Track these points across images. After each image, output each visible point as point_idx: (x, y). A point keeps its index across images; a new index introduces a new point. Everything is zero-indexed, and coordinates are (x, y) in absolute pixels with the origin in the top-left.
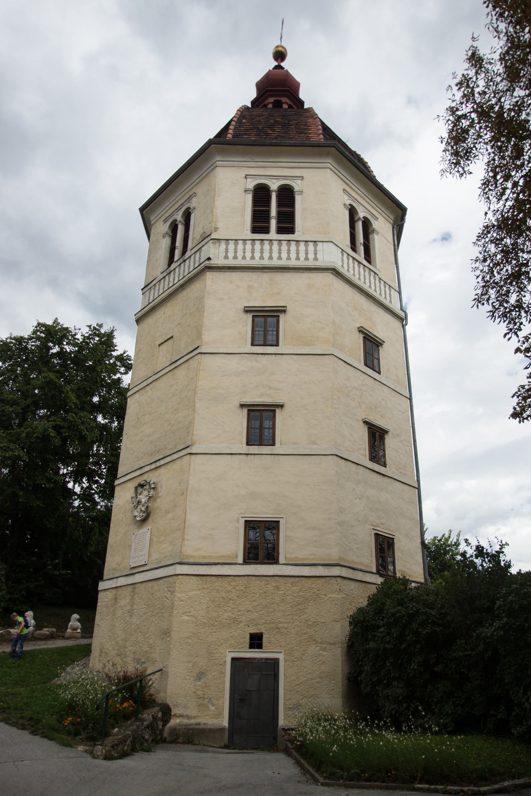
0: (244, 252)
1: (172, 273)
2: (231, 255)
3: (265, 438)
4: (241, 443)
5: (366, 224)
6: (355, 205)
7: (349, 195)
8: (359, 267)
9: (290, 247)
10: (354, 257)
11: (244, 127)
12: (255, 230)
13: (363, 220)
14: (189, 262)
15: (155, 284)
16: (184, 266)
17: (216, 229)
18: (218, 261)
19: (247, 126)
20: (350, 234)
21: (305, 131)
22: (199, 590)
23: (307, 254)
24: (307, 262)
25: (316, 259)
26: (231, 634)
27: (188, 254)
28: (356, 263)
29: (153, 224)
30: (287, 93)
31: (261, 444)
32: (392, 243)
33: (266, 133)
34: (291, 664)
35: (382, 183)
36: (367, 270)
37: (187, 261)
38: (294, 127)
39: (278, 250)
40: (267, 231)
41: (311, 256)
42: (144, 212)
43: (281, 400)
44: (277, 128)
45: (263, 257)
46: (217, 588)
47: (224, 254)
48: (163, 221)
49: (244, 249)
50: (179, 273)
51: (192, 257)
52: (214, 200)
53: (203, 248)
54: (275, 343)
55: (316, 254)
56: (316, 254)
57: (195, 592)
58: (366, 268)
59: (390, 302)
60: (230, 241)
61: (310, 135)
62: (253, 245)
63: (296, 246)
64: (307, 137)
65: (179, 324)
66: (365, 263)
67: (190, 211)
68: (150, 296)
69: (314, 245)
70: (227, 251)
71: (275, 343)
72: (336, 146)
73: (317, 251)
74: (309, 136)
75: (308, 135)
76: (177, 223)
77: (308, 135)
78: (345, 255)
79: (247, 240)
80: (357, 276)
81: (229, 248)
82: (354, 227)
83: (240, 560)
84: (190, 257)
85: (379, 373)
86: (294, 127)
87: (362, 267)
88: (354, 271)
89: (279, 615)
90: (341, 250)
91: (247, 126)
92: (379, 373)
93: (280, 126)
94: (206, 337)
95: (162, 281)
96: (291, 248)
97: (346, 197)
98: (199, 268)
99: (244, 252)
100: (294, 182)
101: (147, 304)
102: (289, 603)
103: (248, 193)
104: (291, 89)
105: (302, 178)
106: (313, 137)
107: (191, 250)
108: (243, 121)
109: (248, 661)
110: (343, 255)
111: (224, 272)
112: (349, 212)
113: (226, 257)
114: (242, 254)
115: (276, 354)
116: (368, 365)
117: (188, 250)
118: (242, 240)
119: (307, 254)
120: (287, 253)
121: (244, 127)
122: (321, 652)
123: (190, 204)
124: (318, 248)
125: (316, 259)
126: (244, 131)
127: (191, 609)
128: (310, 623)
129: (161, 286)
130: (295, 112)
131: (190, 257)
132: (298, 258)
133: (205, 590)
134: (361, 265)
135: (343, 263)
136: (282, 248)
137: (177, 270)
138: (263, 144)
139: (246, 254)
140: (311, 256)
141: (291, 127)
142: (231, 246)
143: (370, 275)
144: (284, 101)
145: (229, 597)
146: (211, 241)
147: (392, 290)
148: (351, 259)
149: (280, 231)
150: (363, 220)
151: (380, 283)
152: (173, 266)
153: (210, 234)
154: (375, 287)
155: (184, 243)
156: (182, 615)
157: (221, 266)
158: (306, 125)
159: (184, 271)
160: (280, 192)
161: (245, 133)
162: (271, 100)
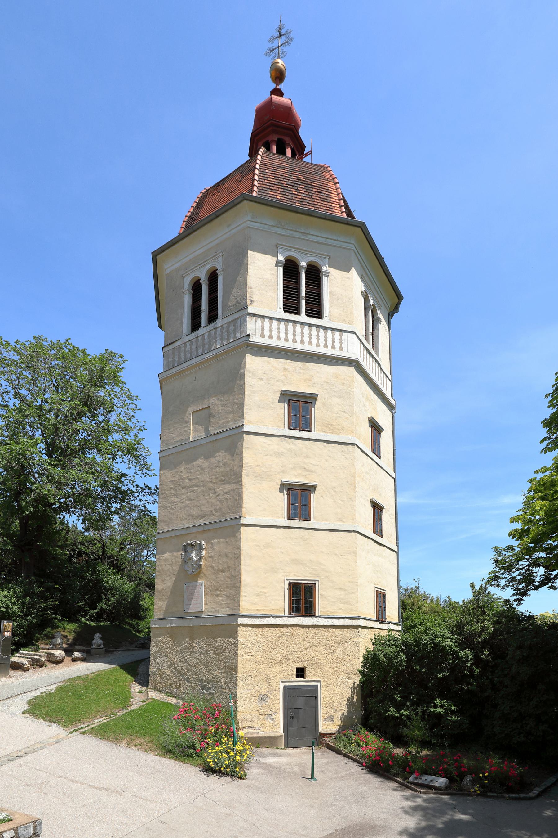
12: (287, 309)
15: (179, 346)
22: (257, 636)
25: (341, 349)
26: (283, 669)
34: (326, 689)
38: (316, 190)
41: (337, 345)
45: (296, 339)
46: (271, 634)
55: (341, 343)
56: (341, 343)
57: (254, 638)
69: (293, 325)
70: (263, 328)
74: (331, 206)
75: (330, 204)
77: (330, 204)
83: (287, 613)
89: (317, 654)
96: (320, 334)
102: (324, 646)
116: (164, 349)
122: (347, 680)
123: (216, 263)
124: (343, 337)
127: (251, 650)
128: (340, 659)
133: (261, 636)
140: (337, 345)
145: (280, 641)
156: (245, 655)
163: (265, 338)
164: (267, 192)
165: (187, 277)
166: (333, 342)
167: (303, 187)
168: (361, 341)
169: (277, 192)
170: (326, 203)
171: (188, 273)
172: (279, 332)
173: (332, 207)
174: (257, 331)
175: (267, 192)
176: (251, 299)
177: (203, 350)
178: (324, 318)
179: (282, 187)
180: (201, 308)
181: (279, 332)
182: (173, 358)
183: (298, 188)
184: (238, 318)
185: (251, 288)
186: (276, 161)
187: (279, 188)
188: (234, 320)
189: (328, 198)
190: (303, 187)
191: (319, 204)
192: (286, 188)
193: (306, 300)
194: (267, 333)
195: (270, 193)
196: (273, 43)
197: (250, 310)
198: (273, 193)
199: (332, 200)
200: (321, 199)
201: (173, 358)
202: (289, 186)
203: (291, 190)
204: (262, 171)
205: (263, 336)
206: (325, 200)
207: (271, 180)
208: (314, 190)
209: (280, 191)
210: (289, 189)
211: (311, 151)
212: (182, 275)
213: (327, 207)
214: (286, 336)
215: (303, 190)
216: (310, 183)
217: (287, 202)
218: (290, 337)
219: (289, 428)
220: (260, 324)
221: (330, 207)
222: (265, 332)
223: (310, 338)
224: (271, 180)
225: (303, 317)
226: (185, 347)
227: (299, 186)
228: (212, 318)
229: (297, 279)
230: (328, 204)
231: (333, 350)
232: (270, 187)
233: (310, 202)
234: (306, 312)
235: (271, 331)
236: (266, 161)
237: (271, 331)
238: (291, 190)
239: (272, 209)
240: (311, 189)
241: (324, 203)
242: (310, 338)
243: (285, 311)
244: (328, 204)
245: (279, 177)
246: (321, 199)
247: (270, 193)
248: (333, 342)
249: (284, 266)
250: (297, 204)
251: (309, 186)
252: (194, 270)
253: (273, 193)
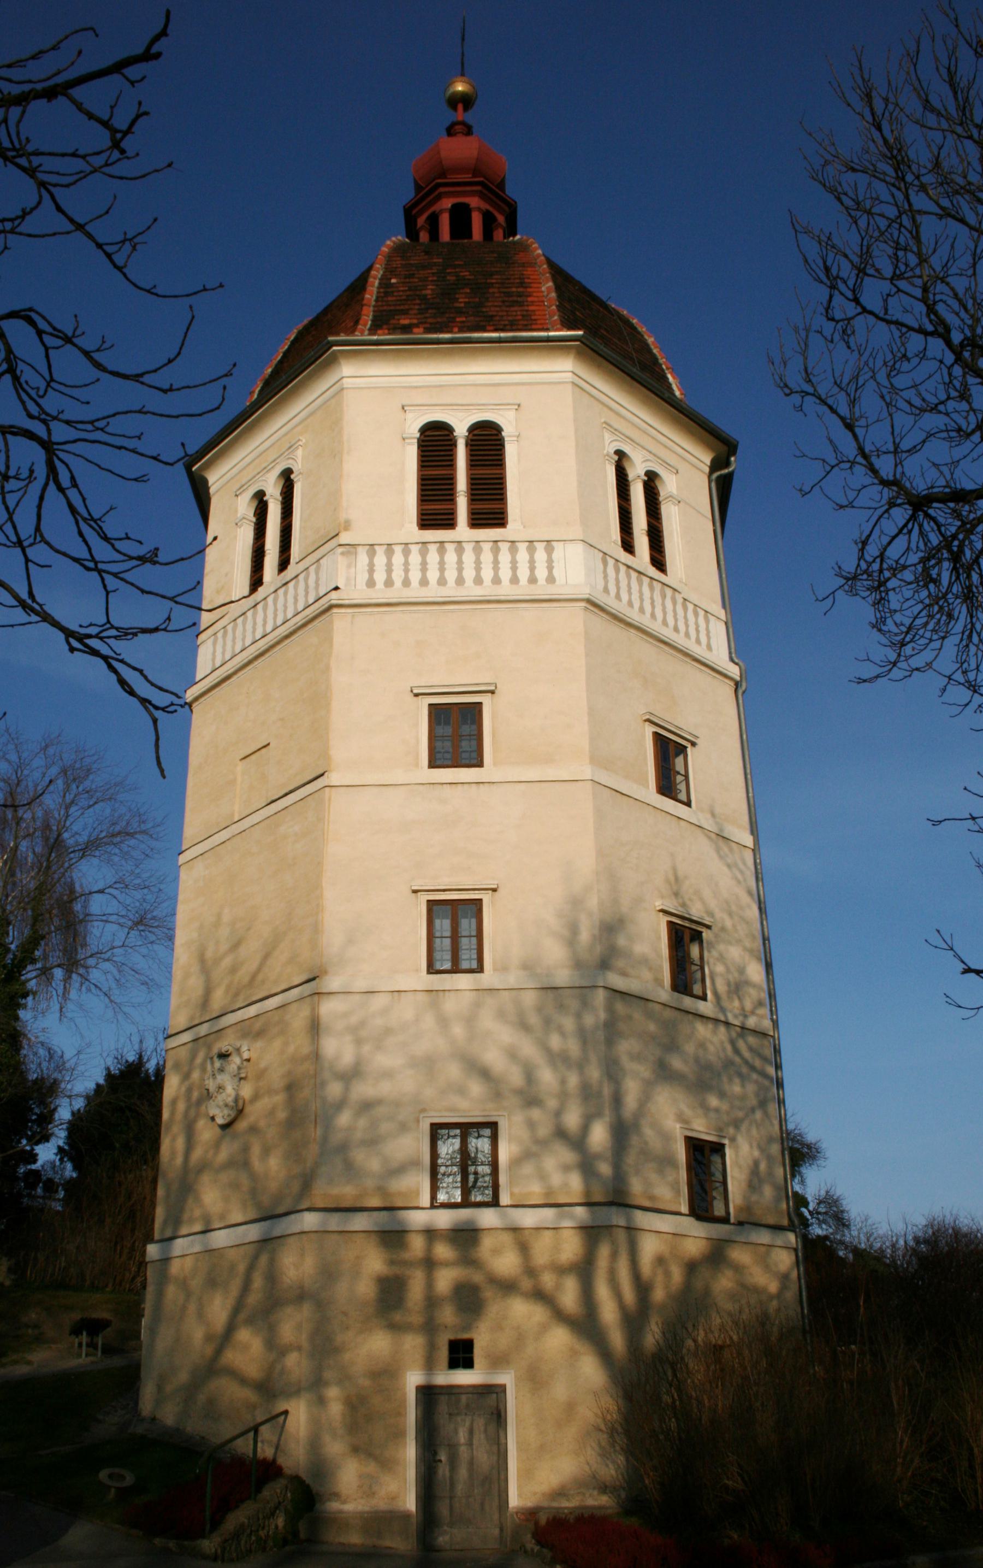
0: (407, 571)
1: (260, 607)
2: (380, 577)
3: (464, 933)
4: (417, 970)
5: (651, 483)
6: (627, 449)
7: (615, 431)
8: (640, 584)
10: (630, 564)
11: (395, 294)
13: (646, 478)
14: (296, 588)
16: (286, 594)
17: (347, 526)
18: (356, 592)
19: (401, 293)
20: (620, 512)
21: (519, 299)
23: (532, 568)
24: (533, 586)
25: (551, 579)
27: (292, 570)
28: (634, 575)
29: (214, 494)
30: (479, 188)
31: (456, 763)
32: (710, 517)
36: (657, 586)
37: (291, 585)
39: (475, 562)
40: (448, 522)
41: (541, 573)
42: (194, 469)
44: (463, 296)
47: (366, 576)
49: (406, 564)
50: (276, 610)
51: (301, 577)
52: (342, 461)
53: (322, 561)
54: (474, 965)
55: (550, 568)
56: (550, 568)
58: (655, 583)
59: (709, 647)
60: (376, 547)
61: (531, 308)
62: (424, 553)
64: (525, 313)
65: (282, 719)
66: (653, 571)
67: (292, 477)
68: (214, 652)
71: (474, 965)
73: (552, 561)
74: (527, 311)
76: (265, 499)
78: (611, 562)
80: (637, 605)
82: (629, 495)
84: (297, 576)
85: (688, 804)
86: (496, 290)
87: (646, 581)
88: (630, 593)
90: (601, 554)
91: (401, 293)
92: (688, 804)
93: (468, 291)
94: (340, 751)
95: (240, 621)
97: (608, 437)
98: (317, 605)
99: (407, 571)
100: (502, 416)
101: (209, 672)
103: (409, 444)
104: (487, 179)
105: (516, 407)
106: (537, 313)
107: (297, 563)
108: (393, 281)
109: (439, 707)
110: (605, 563)
112: (616, 470)
113: (371, 583)
114: (403, 574)
117: (293, 559)
119: (532, 568)
120: (493, 568)
121: (395, 294)
124: (555, 556)
125: (551, 579)
126: (396, 305)
129: (237, 632)
131: (297, 576)
132: (515, 580)
134: (645, 579)
135: (606, 582)
136: (482, 558)
137: (270, 600)
139: (411, 574)
140: (541, 573)
141: (491, 290)
142: (380, 559)
143: (664, 596)
146: (340, 550)
147: (712, 619)
148: (623, 569)
149: (479, 520)
150: (646, 478)
151: (685, 609)
152: (262, 592)
153: (337, 535)
154: (676, 620)
155: (281, 541)
158: (522, 284)
159: (285, 607)
160: (474, 435)
161: (398, 308)
162: (447, 203)
228: (284, 564)
246: (507, 304)
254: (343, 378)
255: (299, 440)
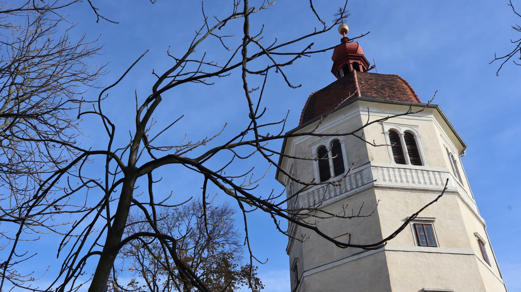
9: (424, 174)
33: (381, 92)
35: (214, 72)
38: (397, 89)
43: (450, 288)
48: (400, 159)
63: (428, 175)
72: (437, 108)
79: (395, 168)
81: (436, 177)
111: (386, 190)
115: (437, 253)
118: (392, 168)
124: (442, 176)
130: (391, 78)
138: (391, 103)
144: (359, 63)
157: (391, 187)
163: (416, 183)
164: (367, 94)
165: (314, 146)
166: (436, 180)
167: (388, 88)
168: (454, 178)
169: (373, 93)
170: (405, 96)
171: (315, 144)
172: (395, 177)
173: (410, 98)
174: (380, 177)
175: (367, 94)
176: (371, 157)
177: (335, 193)
178: (425, 164)
179: (375, 90)
180: (329, 164)
181: (395, 177)
182: (309, 200)
183: (385, 90)
184: (363, 170)
185: (370, 150)
186: (365, 76)
187: (373, 91)
188: (360, 171)
189: (405, 93)
190: (388, 88)
191: (401, 97)
192: (377, 90)
193: (409, 154)
194: (387, 178)
195: (368, 94)
196: (337, 16)
197: (372, 164)
198: (370, 94)
199: (408, 93)
200: (402, 94)
201: (309, 200)
202: (379, 89)
203: (381, 91)
204: (360, 83)
205: (384, 180)
206: (404, 94)
207: (367, 86)
208: (395, 89)
209: (374, 92)
210: (379, 90)
211: (375, 65)
212: (310, 145)
213: (406, 98)
214: (384, 178)
215: (389, 90)
216: (391, 86)
217: (381, 98)
218: (404, 179)
219: (419, 245)
220: (381, 172)
221: (409, 97)
222: (385, 177)
223: (418, 179)
224: (367, 86)
225: (410, 165)
226: (318, 192)
227: (385, 88)
229: (399, 142)
230: (407, 96)
231: (390, 183)
232: (368, 91)
233: (395, 96)
234: (411, 162)
235: (389, 176)
236: (360, 77)
237: (389, 176)
238: (381, 91)
239: (376, 103)
240: (393, 89)
241: (404, 96)
242: (418, 179)
243: (397, 163)
244: (407, 96)
245: (371, 85)
247: (368, 94)
248: (436, 180)
249: (389, 135)
250: (387, 98)
251: (391, 88)
252: (320, 141)
253: (370, 94)
254: (360, 111)
255: (342, 130)
